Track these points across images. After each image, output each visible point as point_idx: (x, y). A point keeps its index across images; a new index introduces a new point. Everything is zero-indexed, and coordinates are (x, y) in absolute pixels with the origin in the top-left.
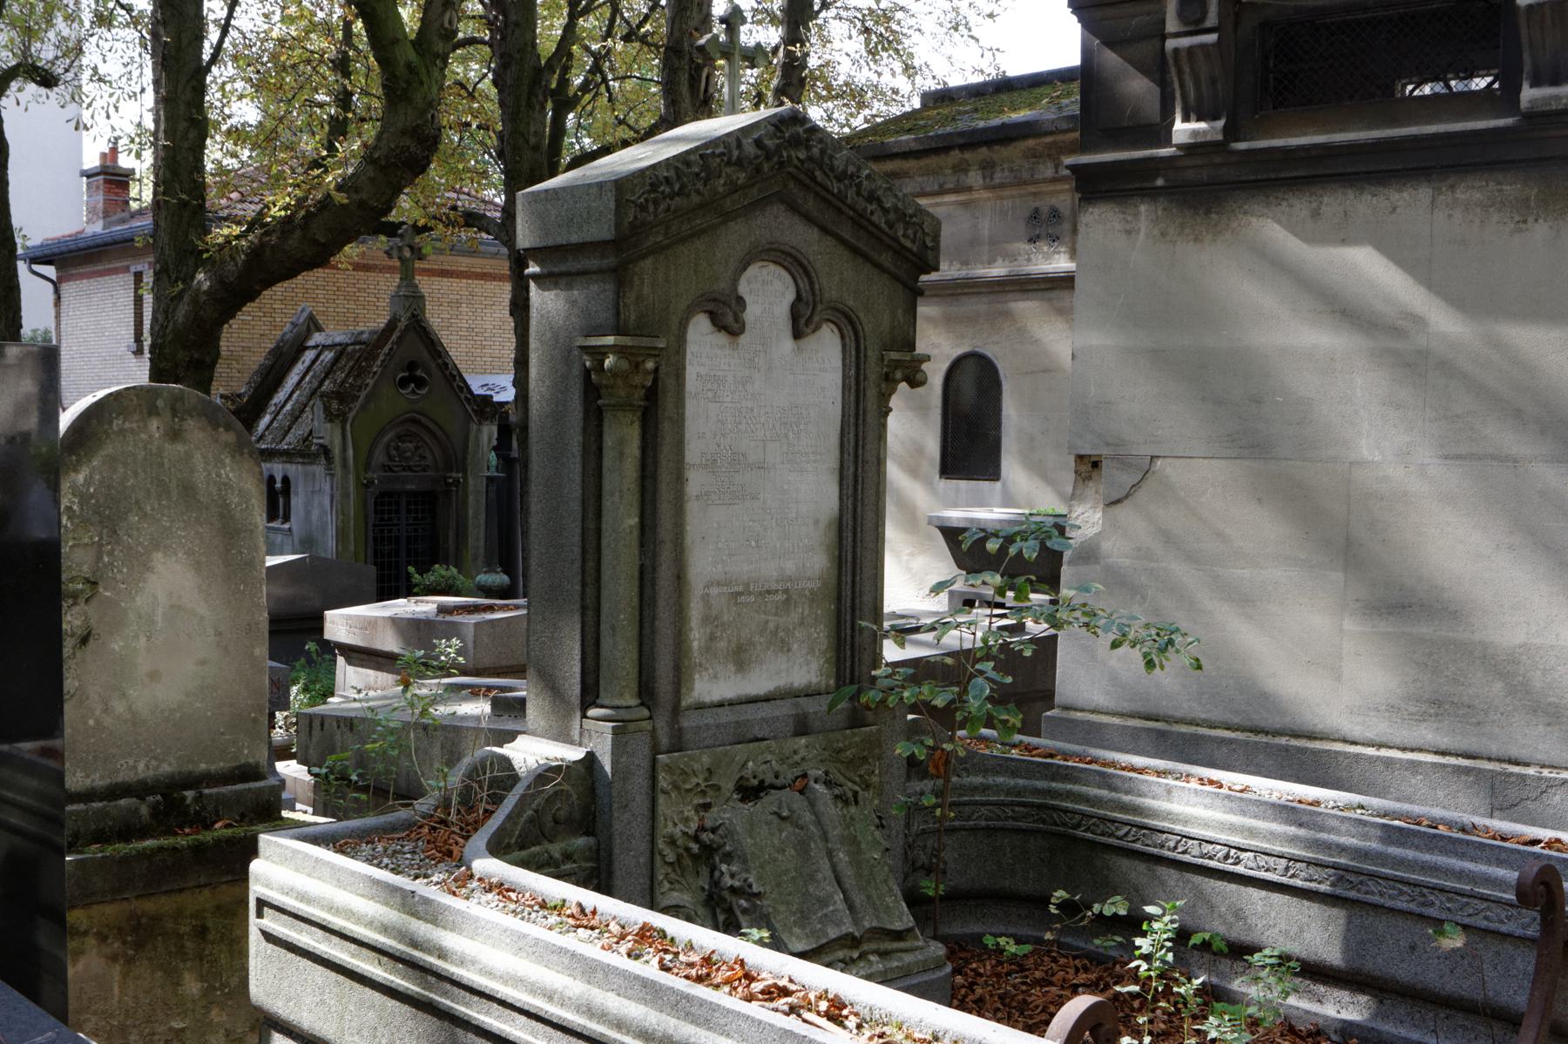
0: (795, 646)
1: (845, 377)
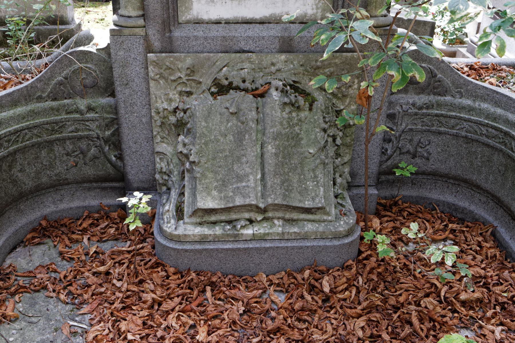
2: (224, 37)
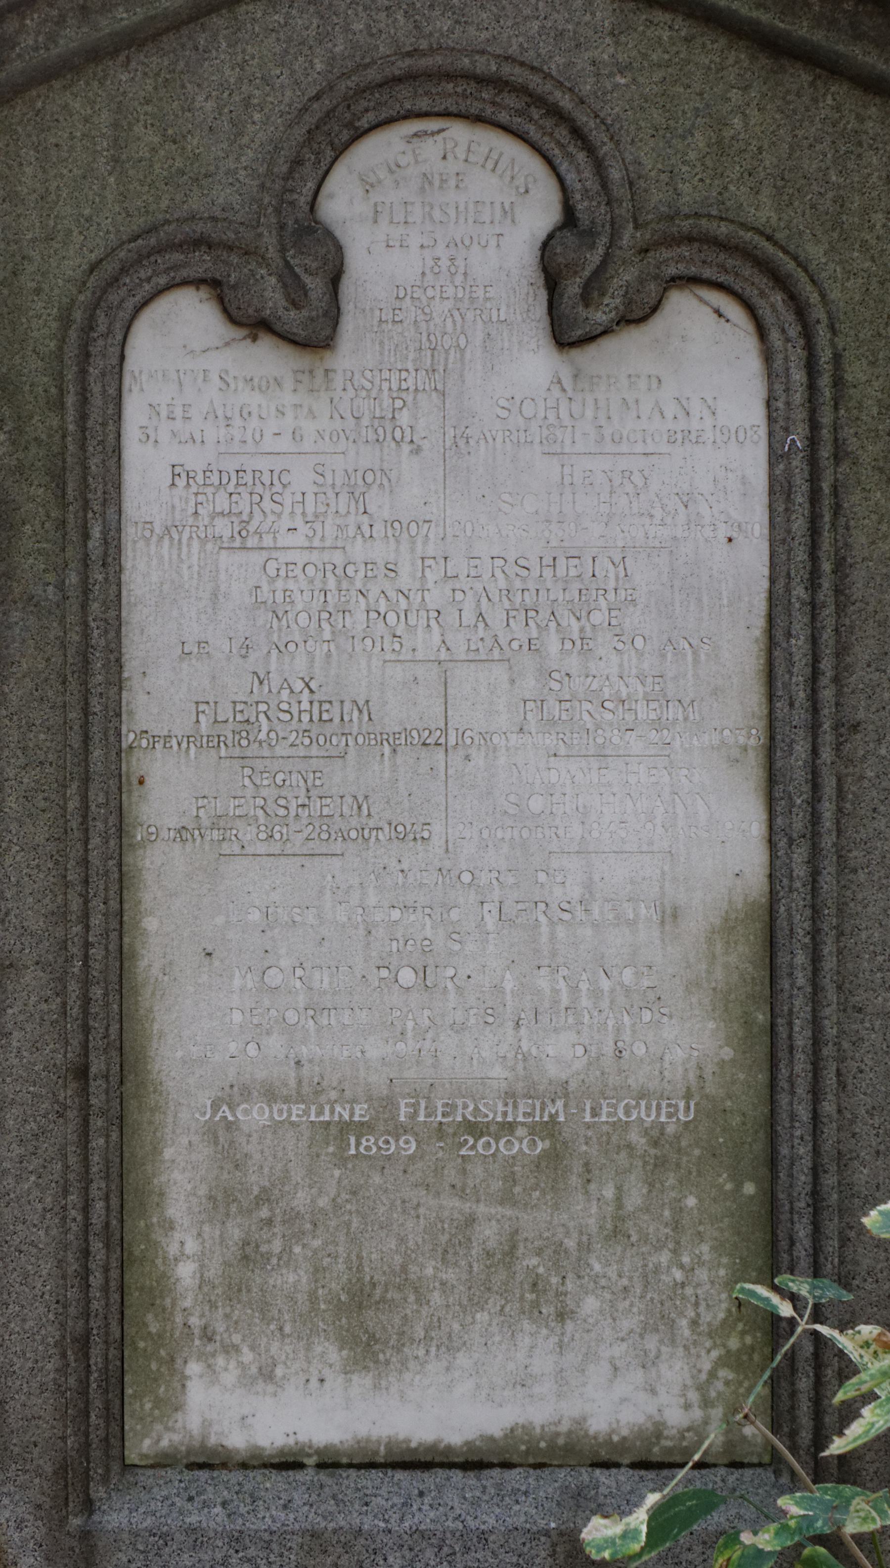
0: (591, 1304)
1: (775, 457)
2: (315, 1535)
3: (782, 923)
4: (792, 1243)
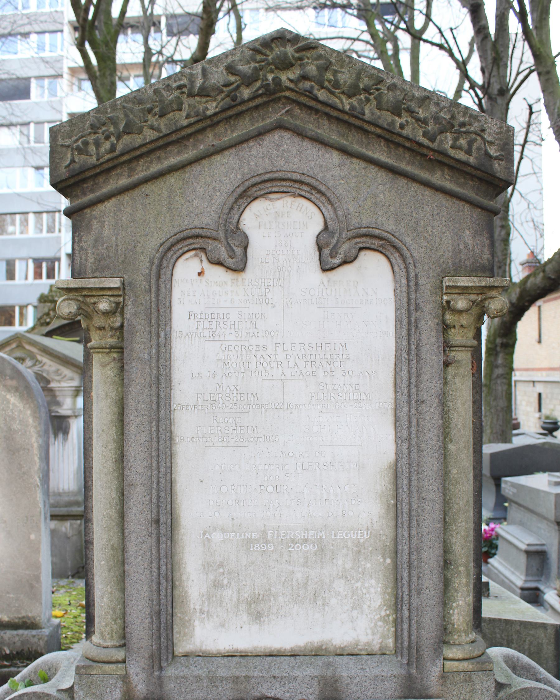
0: (333, 601)
3: (399, 469)
4: (402, 579)
